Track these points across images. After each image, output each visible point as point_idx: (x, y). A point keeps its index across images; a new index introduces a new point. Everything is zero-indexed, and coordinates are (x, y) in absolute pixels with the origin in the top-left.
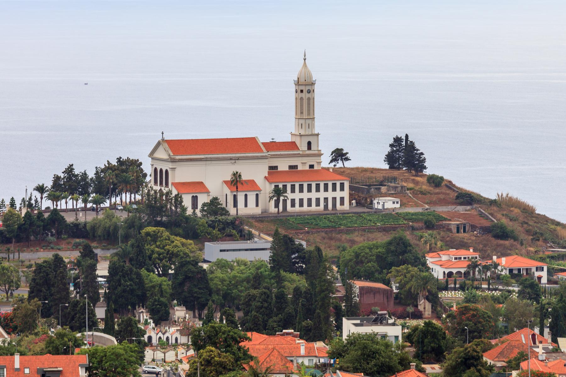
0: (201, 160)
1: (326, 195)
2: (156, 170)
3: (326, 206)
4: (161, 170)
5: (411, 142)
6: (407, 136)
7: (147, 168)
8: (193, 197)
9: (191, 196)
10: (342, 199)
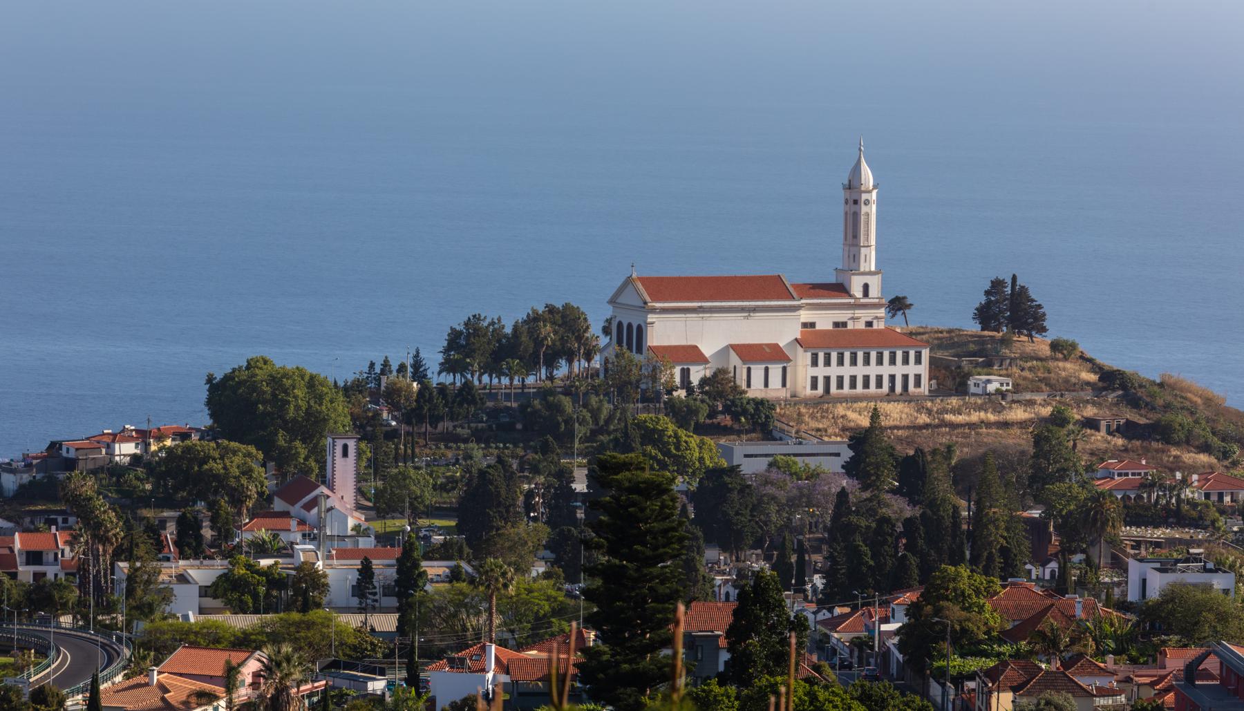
3: (892, 388)
4: (630, 326)
6: (1014, 278)
10: (918, 378)
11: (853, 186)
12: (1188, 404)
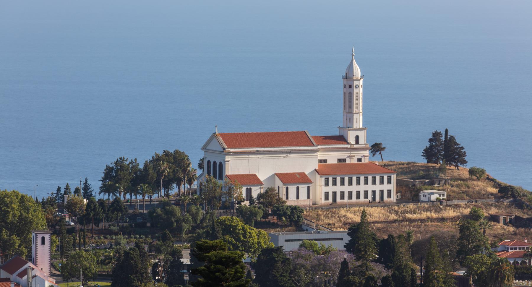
0: (283, 152)
1: (374, 187)
3: (374, 198)
5: (452, 137)
6: (447, 131)
10: (389, 192)
11: (348, 77)
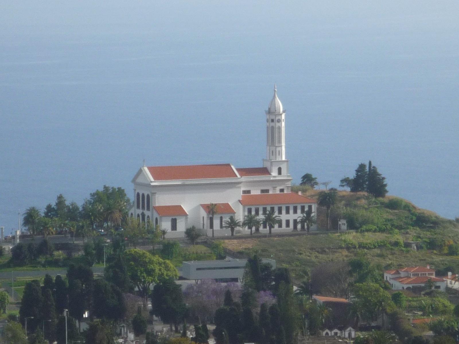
2: (138, 194)
5: (374, 167)
6: (370, 163)
7: (131, 196)
8: (172, 219)
9: (170, 218)
11: (272, 113)
12: (42, 259)
